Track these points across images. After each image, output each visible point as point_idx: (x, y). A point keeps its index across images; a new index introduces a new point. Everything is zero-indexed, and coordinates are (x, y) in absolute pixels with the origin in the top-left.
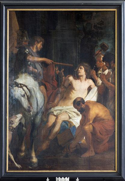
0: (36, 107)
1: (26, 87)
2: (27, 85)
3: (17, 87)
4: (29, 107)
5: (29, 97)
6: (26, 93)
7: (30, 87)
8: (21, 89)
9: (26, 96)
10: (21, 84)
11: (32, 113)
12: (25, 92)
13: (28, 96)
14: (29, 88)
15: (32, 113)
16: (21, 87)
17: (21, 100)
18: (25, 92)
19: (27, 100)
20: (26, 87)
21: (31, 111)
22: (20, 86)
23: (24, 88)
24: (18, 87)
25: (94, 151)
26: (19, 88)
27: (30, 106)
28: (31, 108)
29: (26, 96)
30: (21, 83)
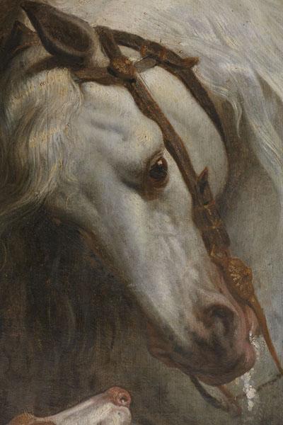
0: (275, 80)
1: (181, 67)
2: (186, 46)
3: (60, 77)
4: (211, 313)
5: (216, 184)
6: (171, 142)
7: (227, 67)
8: (119, 97)
9: (175, 176)
10: (113, 40)
11: (251, 393)
12: (166, 128)
13: (197, 185)
14: (219, 92)
15: (251, 393)
16: (112, 76)
17: (120, 233)
18: (166, 128)
19: (192, 235)
20: (181, 67)
21: (237, 367)
22: (99, 57)
23: (157, 80)
24: (80, 68)
25: (151, 353)
26: (95, 89)
27: (221, 299)
28: (244, 323)
29: (175, 176)
30: (117, 23)
